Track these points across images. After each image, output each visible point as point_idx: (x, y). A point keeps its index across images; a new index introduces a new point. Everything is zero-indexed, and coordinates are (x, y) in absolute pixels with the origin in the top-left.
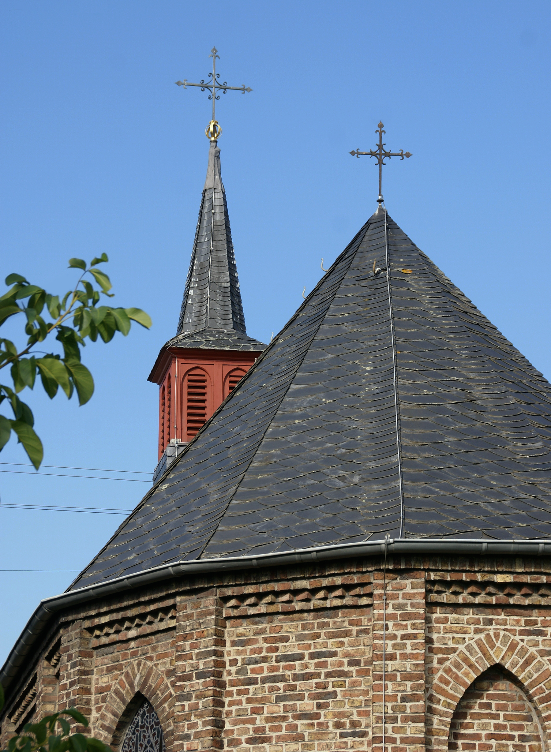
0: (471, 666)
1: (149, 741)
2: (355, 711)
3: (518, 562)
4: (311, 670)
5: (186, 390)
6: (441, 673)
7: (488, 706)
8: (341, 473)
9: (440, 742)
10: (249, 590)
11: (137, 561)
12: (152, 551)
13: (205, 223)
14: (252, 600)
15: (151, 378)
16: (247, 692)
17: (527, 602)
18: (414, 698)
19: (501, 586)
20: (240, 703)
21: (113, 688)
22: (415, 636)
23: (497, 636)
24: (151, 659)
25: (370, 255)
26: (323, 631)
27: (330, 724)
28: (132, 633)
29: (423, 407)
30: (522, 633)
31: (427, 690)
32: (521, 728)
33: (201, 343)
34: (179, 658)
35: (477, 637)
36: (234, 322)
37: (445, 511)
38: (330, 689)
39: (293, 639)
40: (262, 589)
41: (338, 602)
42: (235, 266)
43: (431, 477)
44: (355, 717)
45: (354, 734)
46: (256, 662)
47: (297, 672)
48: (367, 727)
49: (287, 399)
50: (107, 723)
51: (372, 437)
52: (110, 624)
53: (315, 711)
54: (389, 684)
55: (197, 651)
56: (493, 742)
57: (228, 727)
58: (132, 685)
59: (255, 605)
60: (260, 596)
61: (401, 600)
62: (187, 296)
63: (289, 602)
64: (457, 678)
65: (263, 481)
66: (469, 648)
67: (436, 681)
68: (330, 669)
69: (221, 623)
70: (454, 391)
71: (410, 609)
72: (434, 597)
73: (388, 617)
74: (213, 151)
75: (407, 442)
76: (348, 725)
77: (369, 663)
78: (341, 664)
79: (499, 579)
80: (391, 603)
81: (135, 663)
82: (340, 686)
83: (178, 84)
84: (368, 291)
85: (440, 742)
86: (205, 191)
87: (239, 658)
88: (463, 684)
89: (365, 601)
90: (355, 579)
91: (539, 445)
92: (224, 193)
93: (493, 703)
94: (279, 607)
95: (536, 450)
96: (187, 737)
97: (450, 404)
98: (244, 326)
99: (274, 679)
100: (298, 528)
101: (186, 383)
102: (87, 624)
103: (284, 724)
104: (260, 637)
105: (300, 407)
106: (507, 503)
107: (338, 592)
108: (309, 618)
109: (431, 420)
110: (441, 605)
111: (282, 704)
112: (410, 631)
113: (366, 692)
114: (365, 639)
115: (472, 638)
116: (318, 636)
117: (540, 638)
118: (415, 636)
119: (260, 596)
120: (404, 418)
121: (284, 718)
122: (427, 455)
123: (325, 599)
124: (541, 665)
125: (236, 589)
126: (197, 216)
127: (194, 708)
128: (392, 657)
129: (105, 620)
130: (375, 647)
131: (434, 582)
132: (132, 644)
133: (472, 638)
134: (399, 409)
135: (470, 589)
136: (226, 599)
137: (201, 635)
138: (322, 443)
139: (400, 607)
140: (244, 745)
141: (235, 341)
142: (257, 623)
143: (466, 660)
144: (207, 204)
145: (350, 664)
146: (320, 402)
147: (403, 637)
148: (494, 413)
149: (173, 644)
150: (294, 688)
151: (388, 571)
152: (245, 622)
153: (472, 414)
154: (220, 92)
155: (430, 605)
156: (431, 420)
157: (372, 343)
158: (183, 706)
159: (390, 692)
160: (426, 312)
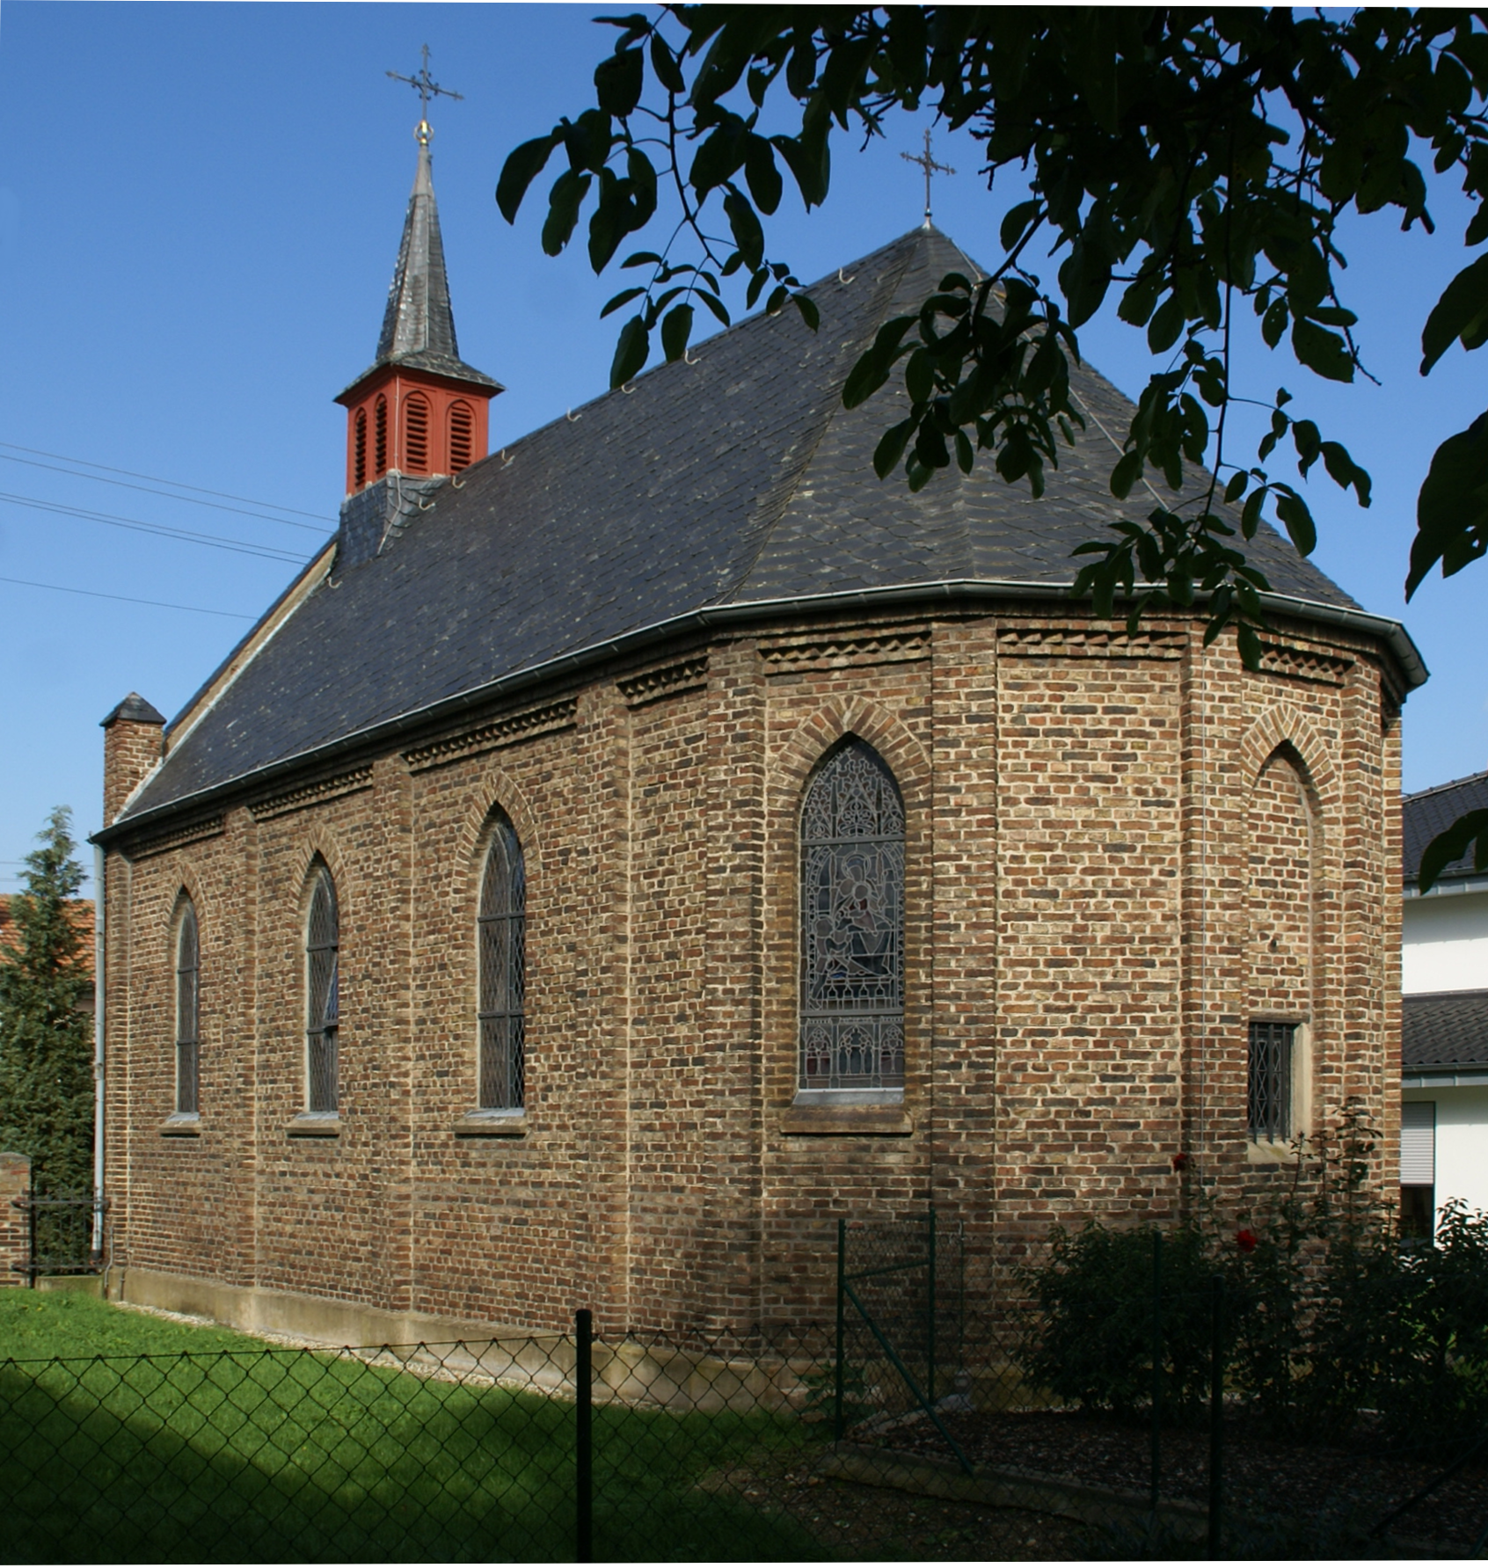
1: (856, 792)
2: (1159, 778)
4: (1105, 726)
17: (1312, 675)
21: (801, 726)
24: (872, 694)
26: (1119, 684)
27: (1130, 790)
28: (840, 661)
38: (1129, 750)
39: (1082, 688)
40: (1052, 625)
41: (1140, 652)
44: (1159, 785)
45: (1158, 804)
46: (1037, 711)
47: (1087, 727)
48: (1174, 796)
50: (793, 766)
52: (802, 648)
53: (1111, 773)
55: (967, 690)
56: (1271, 824)
59: (1037, 643)
60: (1046, 633)
68: (1128, 727)
71: (1227, 669)
76: (1151, 793)
78: (1142, 723)
79: (1299, 646)
81: (842, 698)
82: (1141, 748)
83: (389, 74)
89: (1173, 653)
90: (1168, 627)
93: (1273, 782)
94: (1068, 650)
96: (956, 790)
99: (1060, 733)
102: (765, 644)
103: (1073, 786)
104: (1041, 682)
108: (1102, 666)
111: (1069, 762)
112: (1227, 693)
116: (1113, 688)
119: (1046, 633)
121: (1073, 779)
125: (1019, 621)
129: (794, 642)
132: (837, 675)
139: (1217, 664)
140: (1023, 805)
142: (1037, 665)
145: (1153, 723)
150: (1084, 745)
152: (1021, 663)
154: (431, 93)
158: (947, 754)
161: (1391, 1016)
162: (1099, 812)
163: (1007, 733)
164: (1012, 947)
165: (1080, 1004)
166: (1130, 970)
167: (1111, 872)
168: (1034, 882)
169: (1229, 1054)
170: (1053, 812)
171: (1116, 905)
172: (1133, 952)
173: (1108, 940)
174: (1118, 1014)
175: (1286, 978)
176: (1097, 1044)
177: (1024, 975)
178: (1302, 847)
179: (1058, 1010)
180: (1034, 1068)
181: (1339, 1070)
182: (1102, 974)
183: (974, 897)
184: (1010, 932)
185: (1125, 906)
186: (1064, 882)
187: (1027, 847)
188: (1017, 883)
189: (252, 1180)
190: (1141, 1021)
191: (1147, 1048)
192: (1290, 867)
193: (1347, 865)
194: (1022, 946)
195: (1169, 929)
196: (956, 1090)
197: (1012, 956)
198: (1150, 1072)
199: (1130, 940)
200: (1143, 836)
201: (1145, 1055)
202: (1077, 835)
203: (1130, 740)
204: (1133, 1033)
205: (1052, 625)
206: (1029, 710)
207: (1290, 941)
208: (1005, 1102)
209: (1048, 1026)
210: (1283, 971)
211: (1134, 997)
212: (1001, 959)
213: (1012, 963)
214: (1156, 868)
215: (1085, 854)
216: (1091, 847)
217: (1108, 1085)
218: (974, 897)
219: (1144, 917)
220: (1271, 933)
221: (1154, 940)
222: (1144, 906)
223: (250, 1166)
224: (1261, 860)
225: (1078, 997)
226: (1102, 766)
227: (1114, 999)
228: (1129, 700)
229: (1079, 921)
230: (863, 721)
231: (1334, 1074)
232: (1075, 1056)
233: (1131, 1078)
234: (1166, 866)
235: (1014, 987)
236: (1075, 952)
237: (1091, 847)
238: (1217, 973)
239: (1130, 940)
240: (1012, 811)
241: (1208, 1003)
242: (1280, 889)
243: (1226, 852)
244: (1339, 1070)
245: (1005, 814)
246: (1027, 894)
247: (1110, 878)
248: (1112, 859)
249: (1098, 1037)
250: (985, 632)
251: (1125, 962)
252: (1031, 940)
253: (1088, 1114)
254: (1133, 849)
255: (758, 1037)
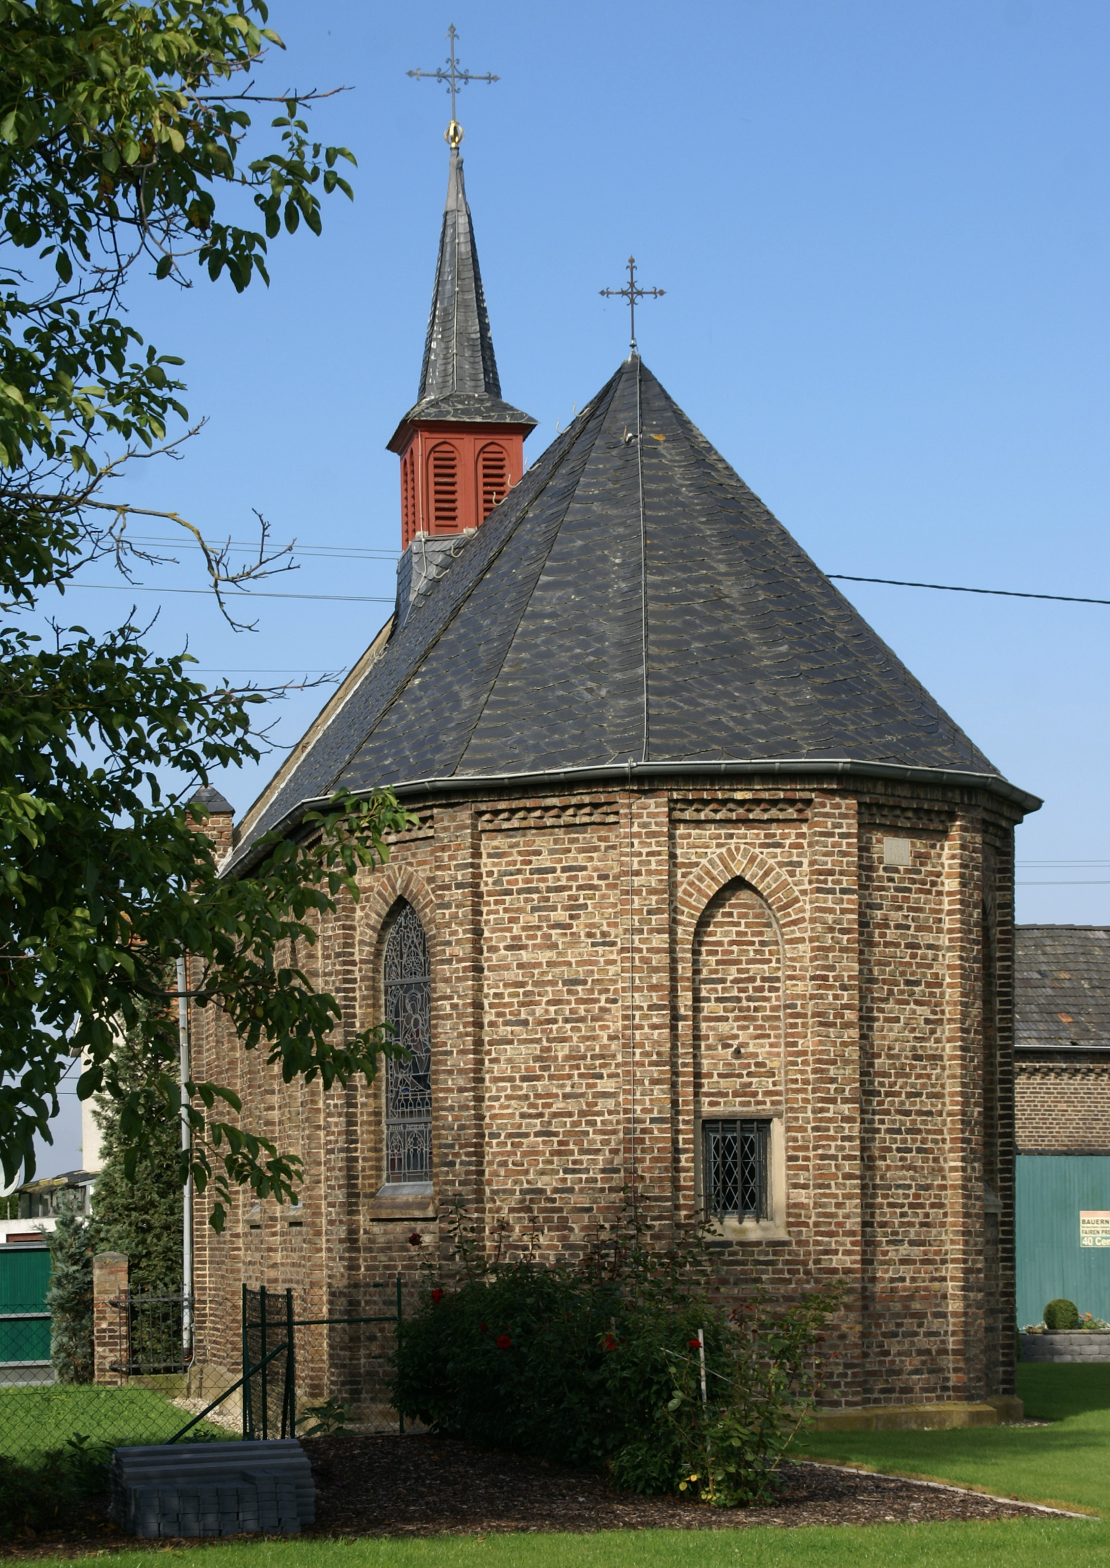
0: (713, 879)
2: (605, 922)
3: (756, 779)
4: (563, 883)
5: (432, 471)
6: (684, 886)
7: (731, 915)
8: (590, 684)
9: (684, 951)
10: (502, 805)
11: (394, 768)
12: (407, 758)
13: (447, 256)
14: (505, 815)
15: (391, 447)
16: (503, 902)
17: (766, 817)
18: (658, 911)
19: (741, 803)
20: (497, 912)
22: (659, 853)
23: (738, 849)
24: (411, 864)
25: (621, 416)
26: (573, 846)
27: (582, 934)
29: (671, 608)
30: (762, 845)
31: (671, 902)
32: (761, 934)
33: (448, 413)
34: (438, 868)
35: (718, 851)
36: (487, 384)
37: (687, 728)
38: (581, 901)
39: (545, 853)
40: (514, 804)
41: (586, 819)
42: (485, 309)
43: (676, 689)
44: (605, 928)
45: (604, 944)
47: (550, 884)
49: (537, 593)
50: (372, 923)
51: (619, 645)
54: (636, 898)
57: (486, 934)
58: (394, 888)
59: (508, 819)
60: (513, 811)
61: (645, 819)
62: (429, 350)
63: (541, 818)
64: (699, 890)
65: (515, 689)
66: (711, 862)
67: (680, 894)
68: (581, 882)
69: (477, 836)
70: (703, 587)
71: (654, 828)
72: (677, 815)
73: (633, 835)
74: (455, 161)
75: (654, 650)
77: (617, 877)
78: (591, 878)
79: (739, 796)
80: (636, 821)
83: (410, 74)
84: (619, 463)
85: (684, 951)
86: (446, 213)
87: (495, 870)
88: (706, 895)
89: (612, 819)
90: (603, 798)
91: (784, 648)
92: (469, 216)
93: (735, 912)
95: (782, 655)
96: (449, 943)
97: (697, 604)
98: (498, 387)
99: (529, 891)
100: (548, 744)
101: (432, 462)
103: (539, 933)
104: (515, 850)
105: (549, 603)
106: (748, 716)
107: (587, 810)
108: (560, 833)
109: (678, 623)
110: (685, 821)
112: (654, 848)
113: (615, 905)
114: (613, 854)
115: (714, 852)
116: (569, 851)
117: (779, 850)
118: (659, 853)
119: (513, 811)
120: (652, 622)
121: (539, 928)
122: (673, 665)
123: (575, 815)
124: (779, 875)
126: (438, 245)
127: (455, 916)
128: (638, 873)
130: (622, 864)
131: (677, 801)
132: (393, 848)
133: (714, 852)
134: (646, 611)
135: (711, 807)
136: (481, 814)
137: (458, 848)
138: (570, 649)
140: (503, 952)
141: (488, 409)
143: (708, 873)
144: (450, 231)
145: (600, 878)
146: (569, 599)
147: (649, 854)
148: (742, 613)
149: (433, 852)
150: (547, 899)
151: (633, 791)
152: (499, 835)
153: (719, 614)
154: (460, 83)
155: (674, 823)
156: (678, 623)
157: (621, 530)
159: (636, 906)
160: (677, 492)
161: (953, 1103)
162: (559, 954)
163: (490, 894)
164: (496, 1066)
165: (547, 1111)
166: (584, 1082)
167: (569, 1002)
168: (511, 1013)
169: (659, 1149)
170: (525, 956)
171: (572, 1029)
172: (586, 1067)
173: (567, 1058)
174: (575, 1118)
175: (754, 1080)
176: (560, 1143)
177: (504, 1089)
178: (774, 964)
179: (530, 1116)
180: (514, 1164)
181: (806, 1159)
182: (563, 1086)
183: (461, 1029)
184: (494, 1055)
185: (579, 1029)
186: (533, 1013)
187: (506, 985)
188: (498, 1015)
189: (239, 1271)
190: (593, 1123)
191: (599, 1146)
192: (758, 983)
193: (813, 978)
194: (503, 1065)
195: (613, 1047)
196: (452, 1183)
197: (496, 1074)
198: (601, 1166)
199: (584, 1057)
200: (592, 972)
201: (597, 1151)
202: (542, 974)
203: (582, 893)
204: (587, 1133)
205: (514, 804)
206: (506, 874)
207: (761, 1049)
208: (493, 1192)
209: (523, 1130)
210: (749, 1074)
211: (588, 1104)
212: (487, 1076)
213: (496, 1080)
214: (603, 997)
215: (549, 989)
216: (553, 983)
217: (569, 1176)
218: (461, 1029)
219: (594, 1038)
220: (735, 1043)
221: (602, 1057)
222: (594, 1029)
223: (235, 1257)
224: (723, 981)
225: (545, 1105)
226: (561, 916)
227: (572, 1106)
228: (581, 859)
229: (545, 1044)
230: (407, 886)
231: (800, 1162)
232: (544, 1153)
233: (587, 1171)
234: (611, 996)
235: (498, 1098)
236: (542, 1068)
237: (553, 983)
238: (647, 1082)
239: (584, 1057)
240: (494, 956)
241: (638, 1108)
242: (745, 1003)
243: (654, 981)
244: (806, 1159)
245: (488, 959)
246: (506, 1023)
247: (567, 1007)
248: (569, 992)
249: (561, 1137)
250: (464, 815)
251: (581, 1076)
252: (509, 1061)
253: (554, 1200)
254: (585, 982)
255: (356, 1141)
